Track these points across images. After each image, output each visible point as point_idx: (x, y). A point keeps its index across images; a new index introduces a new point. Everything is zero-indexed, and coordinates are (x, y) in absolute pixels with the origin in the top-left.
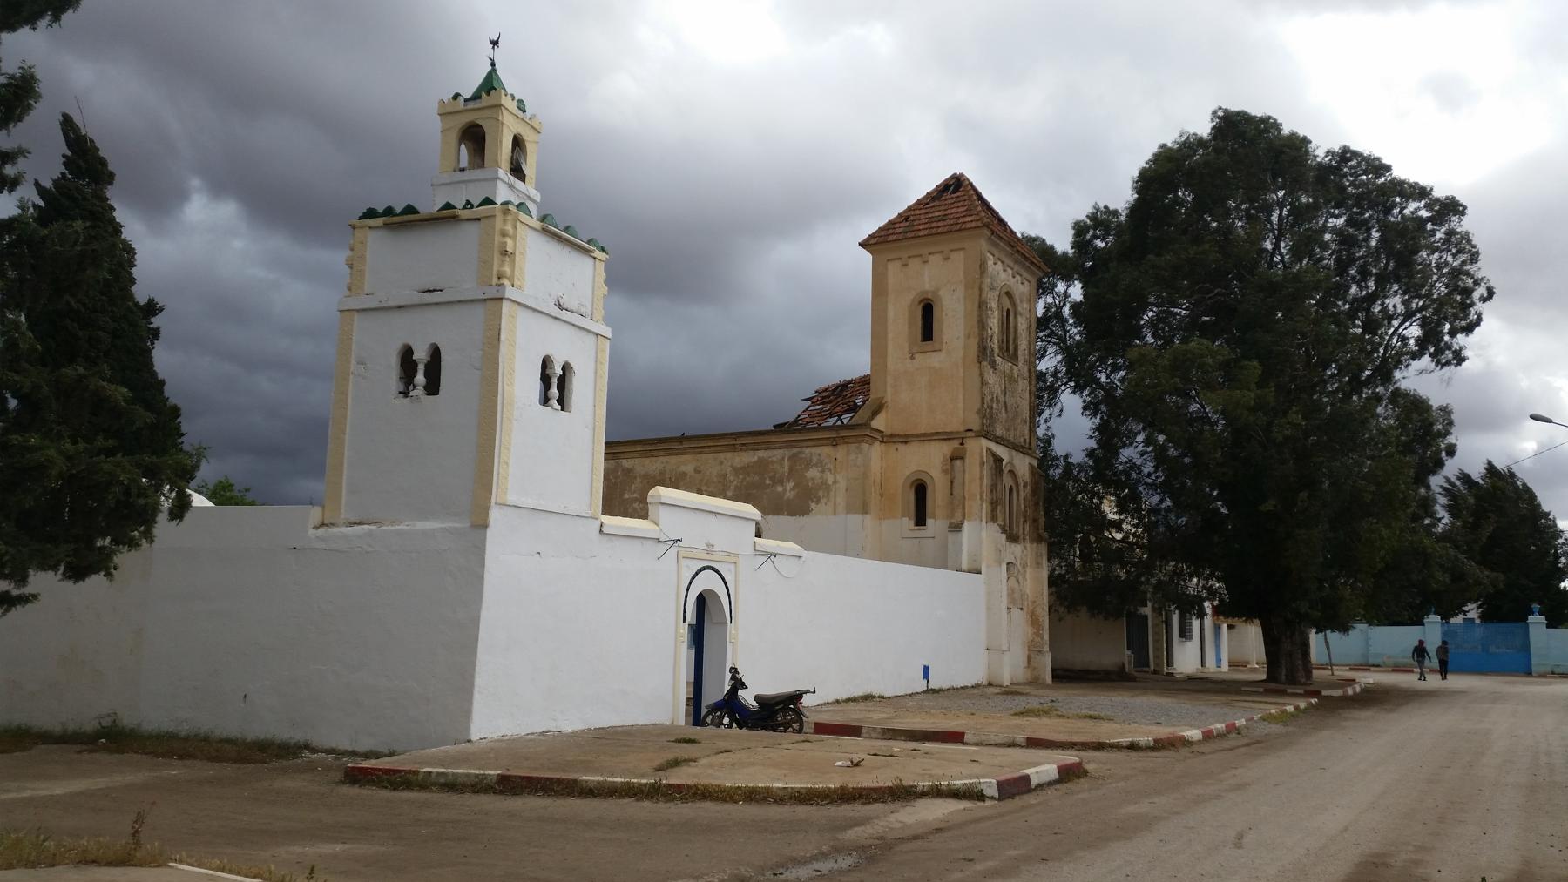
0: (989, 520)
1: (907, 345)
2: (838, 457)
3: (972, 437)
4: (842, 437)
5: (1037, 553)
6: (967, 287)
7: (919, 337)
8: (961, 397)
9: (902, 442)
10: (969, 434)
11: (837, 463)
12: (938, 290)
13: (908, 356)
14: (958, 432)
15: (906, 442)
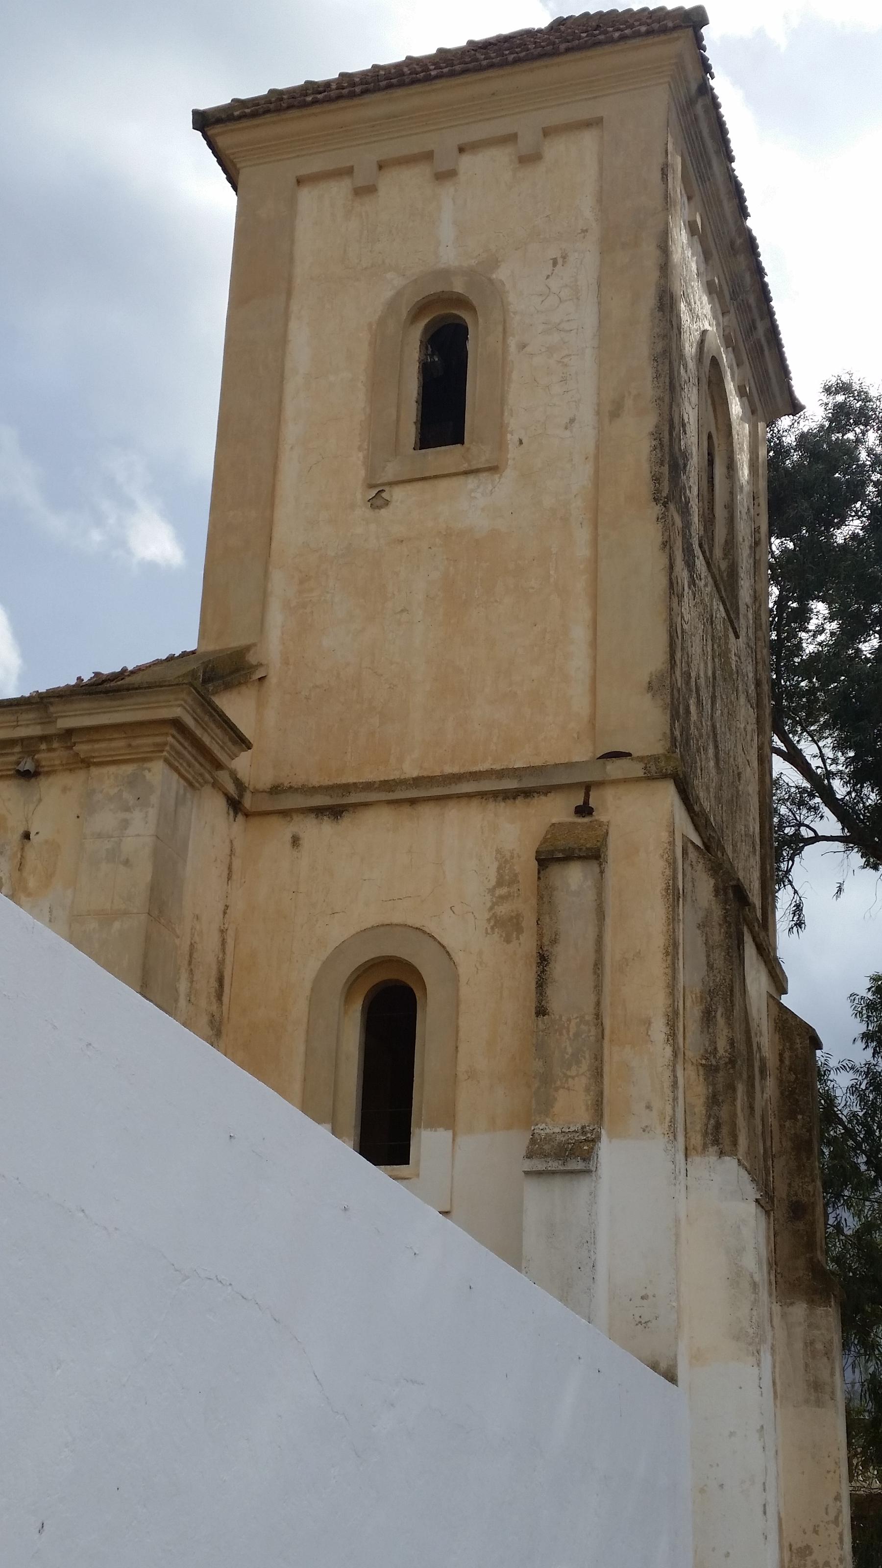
0: (697, 1139)
1: (358, 458)
2: (42, 830)
3: (638, 780)
4: (69, 733)
5: (809, 1344)
6: (606, 246)
7: (410, 432)
8: (580, 633)
9: (319, 812)
10: (614, 769)
11: (31, 854)
12: (494, 263)
13: (360, 495)
14: (570, 765)
15: (336, 812)
